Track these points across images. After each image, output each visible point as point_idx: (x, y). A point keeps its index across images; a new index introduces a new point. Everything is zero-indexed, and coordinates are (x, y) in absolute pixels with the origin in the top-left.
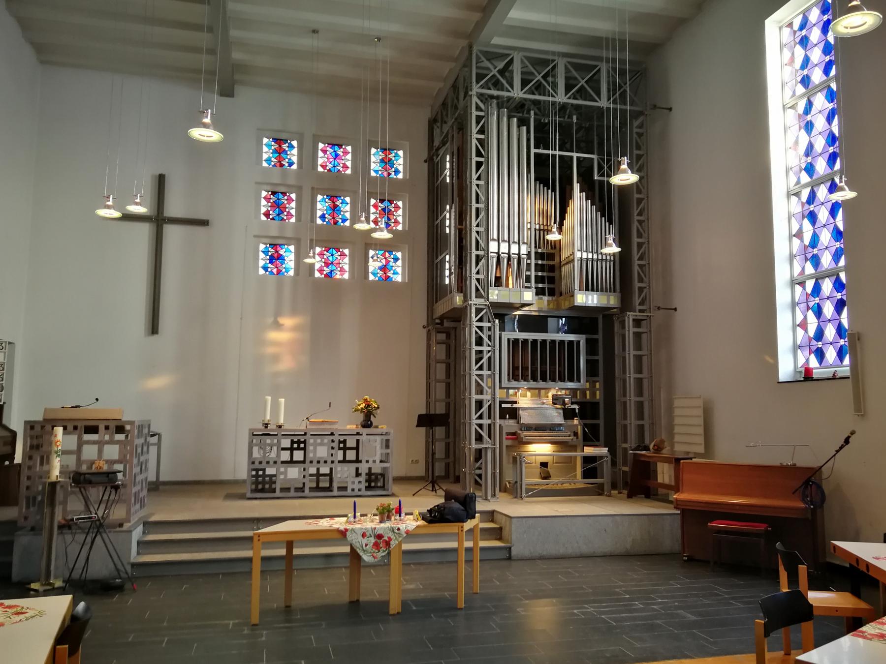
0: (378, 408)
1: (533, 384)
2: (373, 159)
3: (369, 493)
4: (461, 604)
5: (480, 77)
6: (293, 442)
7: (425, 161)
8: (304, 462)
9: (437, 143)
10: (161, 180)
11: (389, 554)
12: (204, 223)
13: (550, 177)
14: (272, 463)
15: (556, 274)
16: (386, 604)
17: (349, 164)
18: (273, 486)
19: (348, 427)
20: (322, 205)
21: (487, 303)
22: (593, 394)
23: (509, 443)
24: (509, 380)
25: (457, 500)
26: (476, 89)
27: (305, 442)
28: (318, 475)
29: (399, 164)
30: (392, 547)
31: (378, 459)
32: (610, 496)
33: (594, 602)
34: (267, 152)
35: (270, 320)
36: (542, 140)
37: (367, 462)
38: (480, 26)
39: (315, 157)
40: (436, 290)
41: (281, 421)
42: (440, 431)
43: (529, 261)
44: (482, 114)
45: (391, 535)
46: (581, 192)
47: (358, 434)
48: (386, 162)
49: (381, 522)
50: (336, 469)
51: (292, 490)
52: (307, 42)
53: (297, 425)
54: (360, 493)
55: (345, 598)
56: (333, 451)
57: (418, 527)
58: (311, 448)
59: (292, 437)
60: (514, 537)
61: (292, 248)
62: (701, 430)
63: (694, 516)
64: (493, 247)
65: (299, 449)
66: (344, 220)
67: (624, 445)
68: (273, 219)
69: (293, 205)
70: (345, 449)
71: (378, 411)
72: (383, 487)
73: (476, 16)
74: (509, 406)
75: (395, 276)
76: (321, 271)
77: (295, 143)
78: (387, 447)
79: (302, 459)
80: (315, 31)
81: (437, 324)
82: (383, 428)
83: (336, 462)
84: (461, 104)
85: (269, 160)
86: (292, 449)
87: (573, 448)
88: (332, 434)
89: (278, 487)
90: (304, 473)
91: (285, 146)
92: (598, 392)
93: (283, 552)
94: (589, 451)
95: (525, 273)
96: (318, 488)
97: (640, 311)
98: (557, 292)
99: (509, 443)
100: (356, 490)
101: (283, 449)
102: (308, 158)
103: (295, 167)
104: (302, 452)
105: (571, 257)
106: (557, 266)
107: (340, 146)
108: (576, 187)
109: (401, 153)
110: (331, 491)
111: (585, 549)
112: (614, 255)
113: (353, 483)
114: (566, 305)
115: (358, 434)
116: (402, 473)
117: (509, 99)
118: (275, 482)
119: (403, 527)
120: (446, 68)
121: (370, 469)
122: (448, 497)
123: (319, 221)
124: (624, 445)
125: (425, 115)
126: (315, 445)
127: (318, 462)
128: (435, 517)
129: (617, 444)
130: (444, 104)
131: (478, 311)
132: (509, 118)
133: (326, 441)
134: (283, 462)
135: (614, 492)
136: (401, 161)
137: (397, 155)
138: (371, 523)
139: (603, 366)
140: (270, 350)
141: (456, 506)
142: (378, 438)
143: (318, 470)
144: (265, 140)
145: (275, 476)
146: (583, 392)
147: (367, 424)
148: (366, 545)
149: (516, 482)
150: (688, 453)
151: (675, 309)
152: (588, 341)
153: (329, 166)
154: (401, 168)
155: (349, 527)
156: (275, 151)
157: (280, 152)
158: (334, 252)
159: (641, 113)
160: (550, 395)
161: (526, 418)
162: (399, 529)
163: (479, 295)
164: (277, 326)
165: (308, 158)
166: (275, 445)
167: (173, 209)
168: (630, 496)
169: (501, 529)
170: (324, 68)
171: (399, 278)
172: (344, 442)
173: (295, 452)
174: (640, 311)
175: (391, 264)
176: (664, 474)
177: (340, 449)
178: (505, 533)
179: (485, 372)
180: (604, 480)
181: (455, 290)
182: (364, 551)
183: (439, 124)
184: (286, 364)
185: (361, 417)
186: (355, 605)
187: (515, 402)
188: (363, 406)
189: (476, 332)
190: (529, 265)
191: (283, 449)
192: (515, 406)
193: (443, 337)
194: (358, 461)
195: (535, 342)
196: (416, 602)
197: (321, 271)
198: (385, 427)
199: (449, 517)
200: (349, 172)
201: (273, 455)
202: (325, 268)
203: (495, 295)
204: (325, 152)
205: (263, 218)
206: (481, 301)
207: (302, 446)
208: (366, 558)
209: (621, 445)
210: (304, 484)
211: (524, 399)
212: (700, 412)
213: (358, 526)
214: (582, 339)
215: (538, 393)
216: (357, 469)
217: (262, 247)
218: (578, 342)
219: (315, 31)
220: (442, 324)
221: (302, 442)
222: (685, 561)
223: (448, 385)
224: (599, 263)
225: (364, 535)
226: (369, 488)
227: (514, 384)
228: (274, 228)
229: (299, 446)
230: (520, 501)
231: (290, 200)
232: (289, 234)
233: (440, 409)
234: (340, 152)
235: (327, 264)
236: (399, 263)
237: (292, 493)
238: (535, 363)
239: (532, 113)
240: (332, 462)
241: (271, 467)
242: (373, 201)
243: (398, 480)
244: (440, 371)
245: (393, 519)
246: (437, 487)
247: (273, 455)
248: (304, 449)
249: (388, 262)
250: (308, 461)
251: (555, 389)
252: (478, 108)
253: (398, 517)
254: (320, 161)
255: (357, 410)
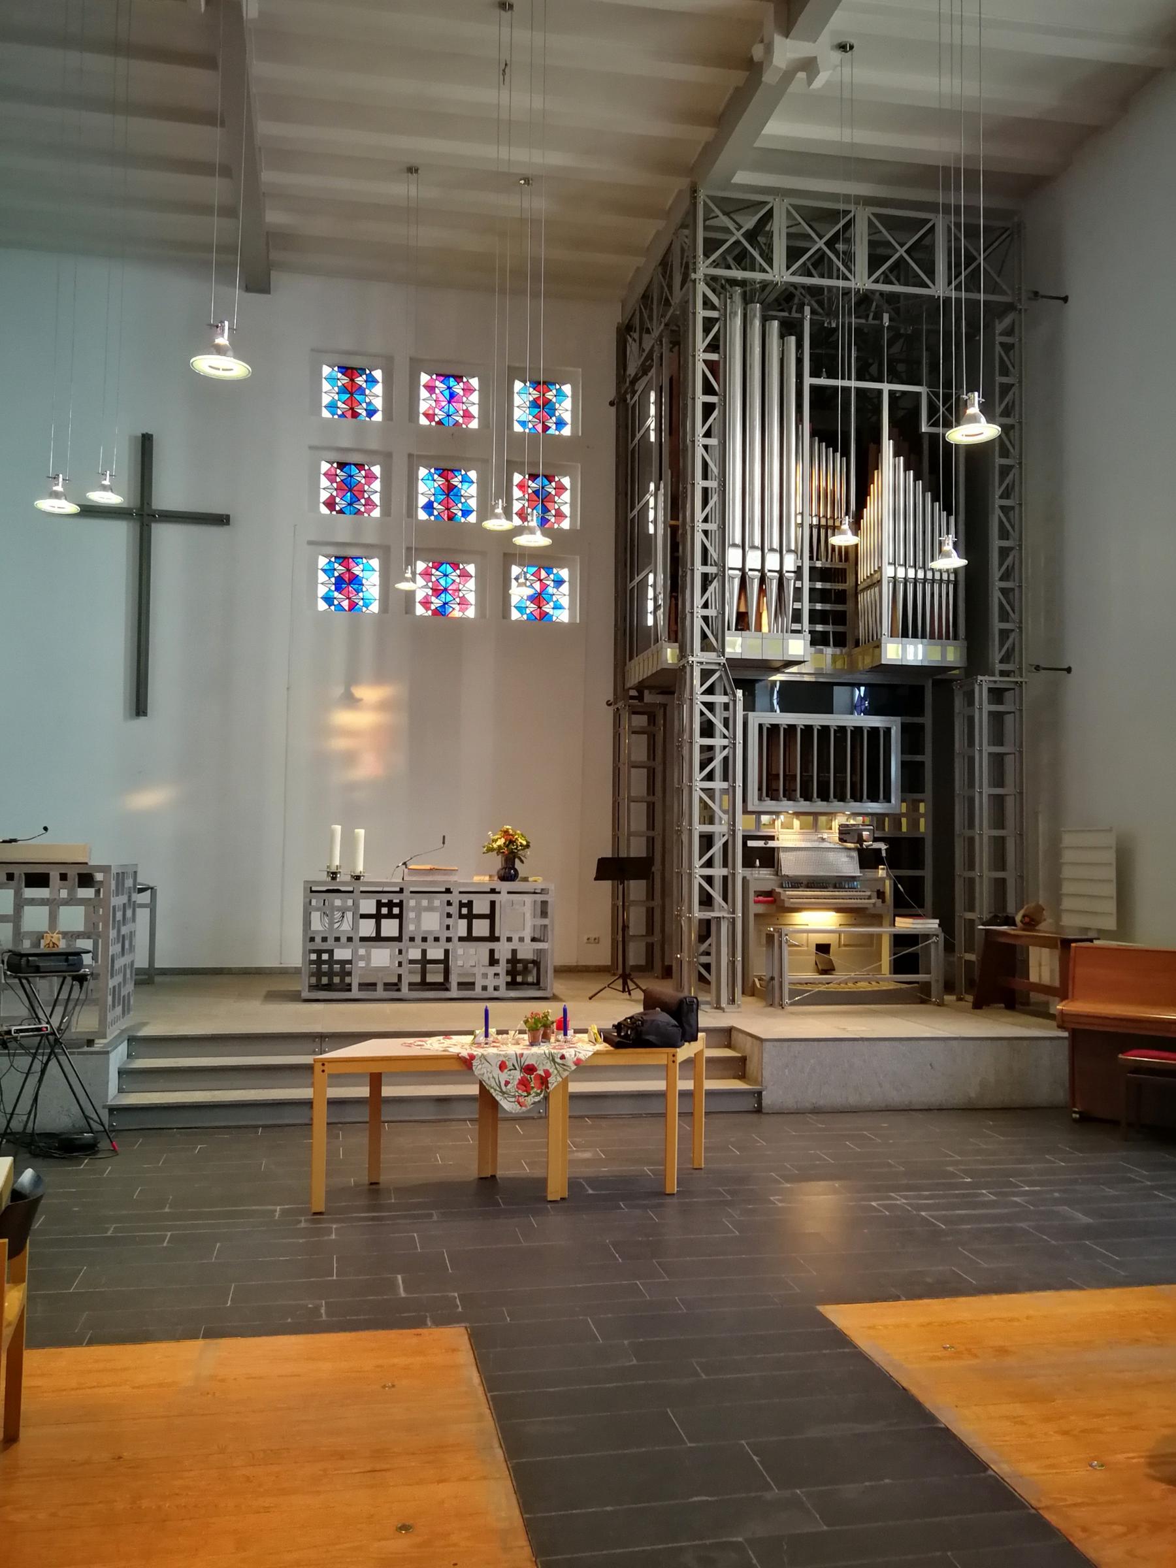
0: (528, 846)
1: (804, 806)
2: (517, 400)
3: (513, 994)
4: (673, 1187)
5: (711, 246)
6: (379, 905)
7: (612, 404)
8: (399, 939)
9: (632, 370)
10: (146, 443)
11: (546, 1098)
12: (222, 520)
13: (843, 431)
14: (344, 940)
15: (848, 607)
16: (542, 1183)
17: (474, 410)
18: (347, 980)
19: (476, 879)
20: (427, 487)
21: (723, 660)
22: (914, 824)
23: (760, 909)
24: (760, 799)
25: (666, 1008)
26: (703, 268)
27: (400, 905)
28: (424, 961)
29: (565, 409)
30: (551, 1087)
31: (527, 934)
32: (941, 1004)
33: (909, 1188)
34: (329, 393)
35: (339, 691)
36: (824, 363)
37: (509, 939)
38: (711, 150)
39: (414, 399)
40: (629, 637)
41: (360, 868)
42: (636, 888)
43: (798, 584)
44: (714, 314)
45: (549, 1066)
46: (897, 454)
47: (493, 891)
48: (543, 406)
49: (532, 1044)
50: (455, 950)
51: (380, 987)
52: (400, 190)
53: (387, 875)
54: (496, 994)
55: (471, 1171)
56: (450, 921)
57: (596, 1054)
58: (412, 915)
59: (379, 897)
60: (766, 1074)
61: (375, 563)
62: (1111, 890)
63: (1090, 1042)
64: (734, 558)
65: (390, 916)
66: (466, 513)
67: (969, 916)
68: (341, 512)
69: (376, 485)
70: (470, 917)
71: (528, 852)
72: (537, 984)
73: (705, 134)
74: (760, 844)
75: (557, 613)
76: (426, 603)
77: (378, 374)
78: (544, 914)
79: (397, 935)
80: (412, 170)
81: (632, 698)
82: (537, 881)
83: (455, 940)
84: (677, 296)
85: (332, 407)
86: (378, 917)
87: (875, 919)
88: (448, 891)
89: (355, 982)
90: (400, 958)
91: (360, 381)
92: (922, 821)
93: (364, 1092)
94: (904, 924)
95: (791, 605)
96: (424, 985)
97: (1003, 673)
98: (850, 641)
99: (760, 909)
100: (491, 989)
101: (363, 916)
102: (402, 401)
103: (378, 417)
104: (397, 921)
105: (877, 576)
106: (850, 592)
107: (459, 379)
108: (888, 446)
109: (567, 389)
110: (447, 990)
111: (896, 1097)
112: (956, 571)
113: (485, 976)
114: (866, 662)
115: (493, 891)
116: (571, 960)
117: (765, 285)
118: (349, 974)
119: (569, 1053)
120: (649, 230)
121: (514, 952)
122: (650, 1002)
123: (422, 515)
124: (969, 916)
125: (610, 318)
126: (419, 910)
127: (424, 939)
128: (627, 1037)
129: (954, 916)
130: (646, 297)
131: (706, 674)
132: (765, 320)
133: (437, 903)
134: (363, 939)
135: (950, 998)
136: (567, 404)
137: (559, 393)
138: (515, 1046)
139: (932, 771)
140: (340, 744)
141: (663, 1018)
142: (528, 899)
143: (424, 952)
144: (326, 370)
145: (350, 962)
146: (896, 819)
147: (508, 874)
148: (507, 1083)
149: (772, 978)
150: (1087, 929)
151: (1069, 670)
152: (905, 728)
153: (440, 415)
154: (567, 417)
155: (477, 1052)
156: (344, 390)
157: (352, 390)
158: (449, 569)
159: (1010, 307)
160: (835, 825)
161: (790, 866)
162: (563, 1057)
163: (706, 646)
164: (351, 701)
165: (402, 401)
166: (348, 909)
167: (167, 497)
168: (978, 1005)
169: (744, 1059)
170: (427, 236)
171: (563, 616)
172: (469, 905)
173: (383, 921)
174: (1003, 673)
175: (550, 590)
176: (1042, 966)
177: (461, 916)
178: (752, 1067)
179: (718, 785)
180: (932, 975)
181: (665, 636)
182: (503, 1093)
183: (636, 335)
184: (368, 768)
185: (497, 862)
186: (488, 1184)
187: (772, 838)
188: (501, 842)
189: (702, 713)
190: (798, 591)
191: (363, 916)
192: (771, 844)
193: (641, 721)
194: (493, 938)
195: (808, 729)
196: (594, 1182)
197: (426, 603)
198: (540, 879)
199: (651, 1038)
200: (474, 425)
201: (346, 926)
202: (433, 599)
203: (736, 645)
204: (431, 389)
205: (324, 510)
206: (711, 656)
207: (396, 911)
208: (507, 1105)
209: (962, 915)
210: (400, 976)
211: (789, 833)
212: (1110, 856)
213: (491, 1051)
214: (893, 724)
215: (813, 821)
216: (492, 952)
217: (322, 562)
218: (888, 731)
219: (412, 170)
220: (640, 697)
221: (396, 905)
222: (1075, 1120)
223: (651, 807)
224: (928, 587)
225: (502, 1066)
226: (512, 985)
227: (769, 805)
228: (343, 528)
229: (390, 911)
230: (780, 1011)
231: (370, 477)
232: (370, 538)
233: (637, 849)
234: (458, 389)
235: (437, 592)
236: (565, 588)
237: (380, 992)
238: (807, 768)
239: (807, 309)
240: (449, 940)
241: (343, 947)
242: (517, 478)
243: (564, 971)
244: (637, 781)
245: (553, 1039)
246: (631, 986)
247: (346, 926)
248: (400, 917)
249: (544, 587)
250: (405, 937)
251: (844, 815)
252: (708, 305)
253: (561, 1037)
254: (423, 407)
255: (492, 850)
